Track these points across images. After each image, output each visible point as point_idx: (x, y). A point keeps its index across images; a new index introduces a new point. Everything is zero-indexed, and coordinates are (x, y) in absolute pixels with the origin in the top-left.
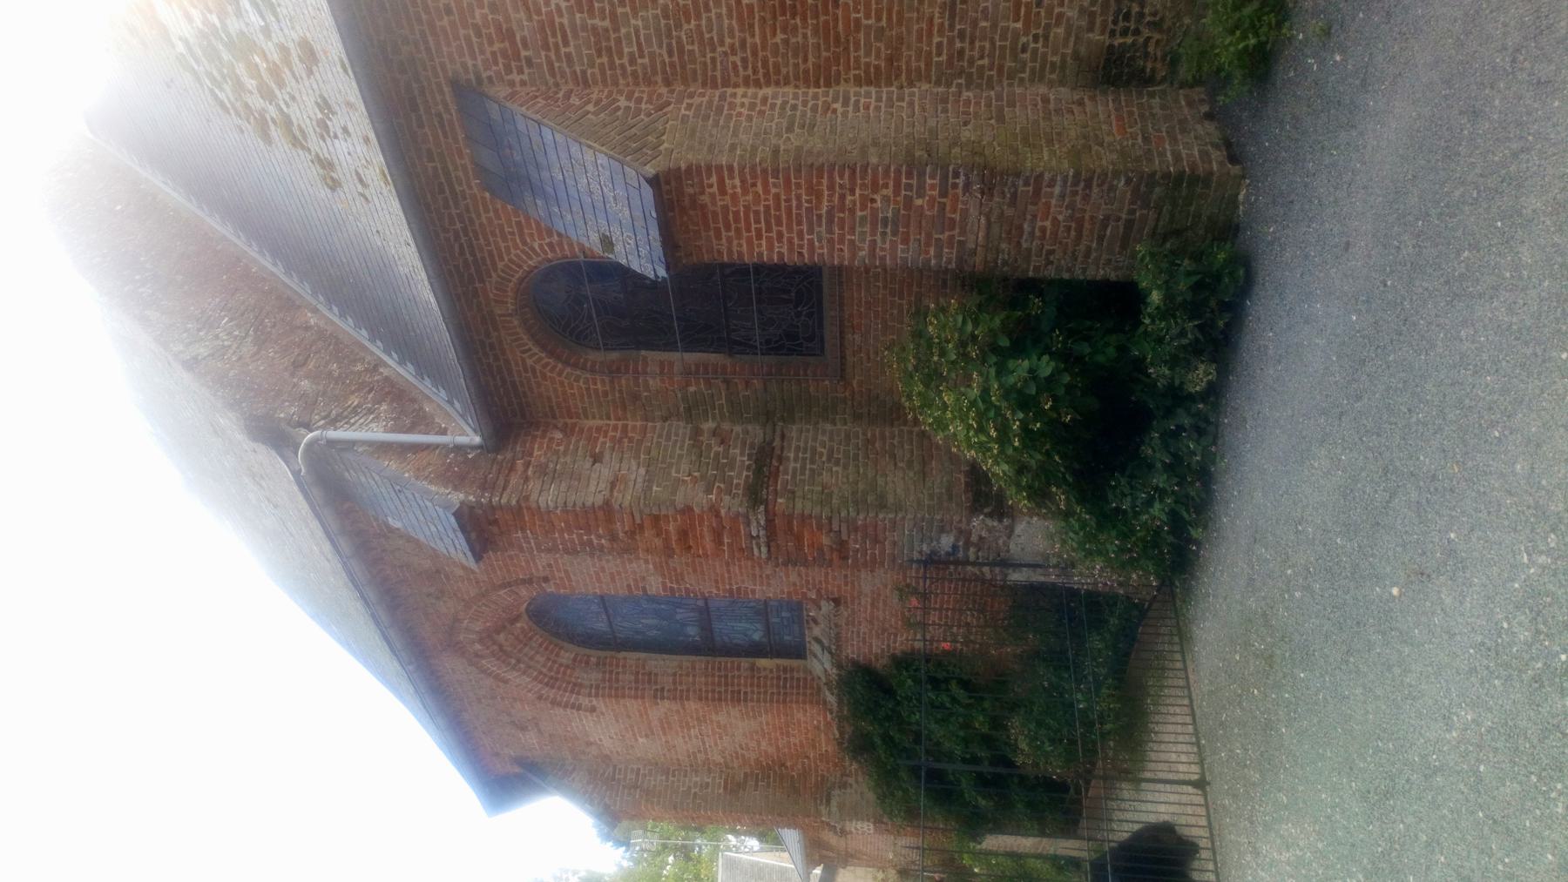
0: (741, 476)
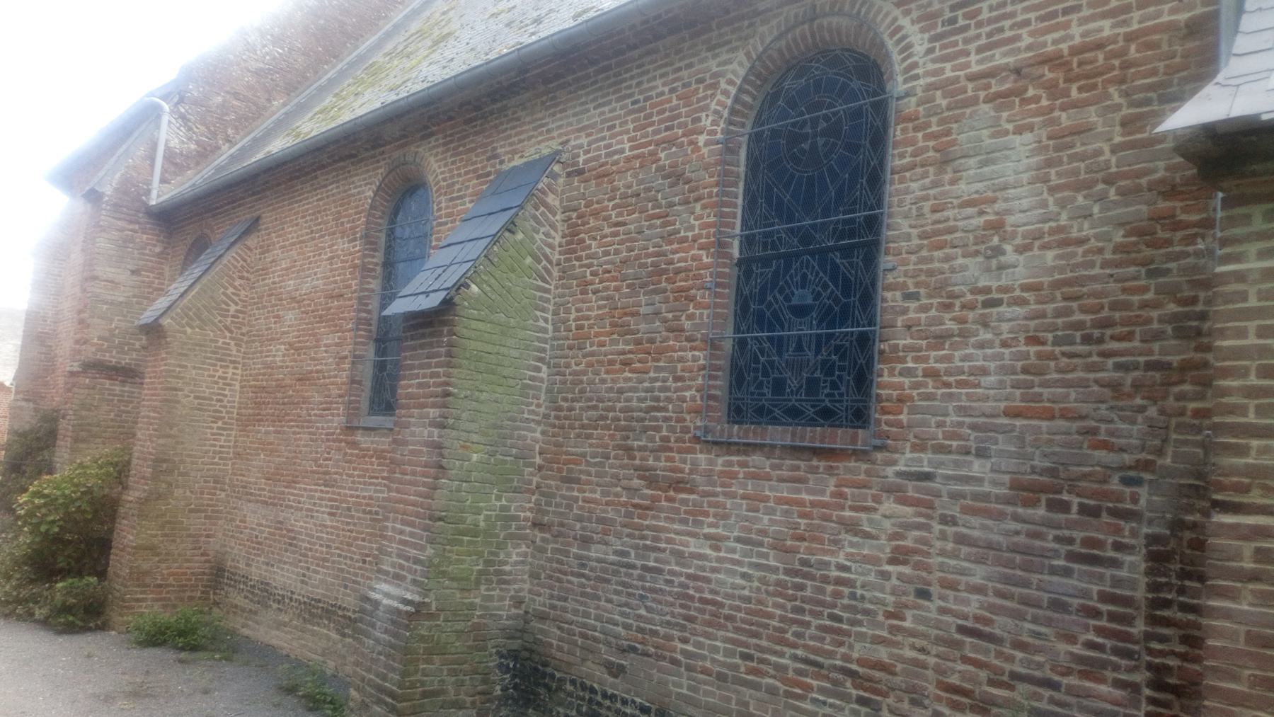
0: (112, 358)
